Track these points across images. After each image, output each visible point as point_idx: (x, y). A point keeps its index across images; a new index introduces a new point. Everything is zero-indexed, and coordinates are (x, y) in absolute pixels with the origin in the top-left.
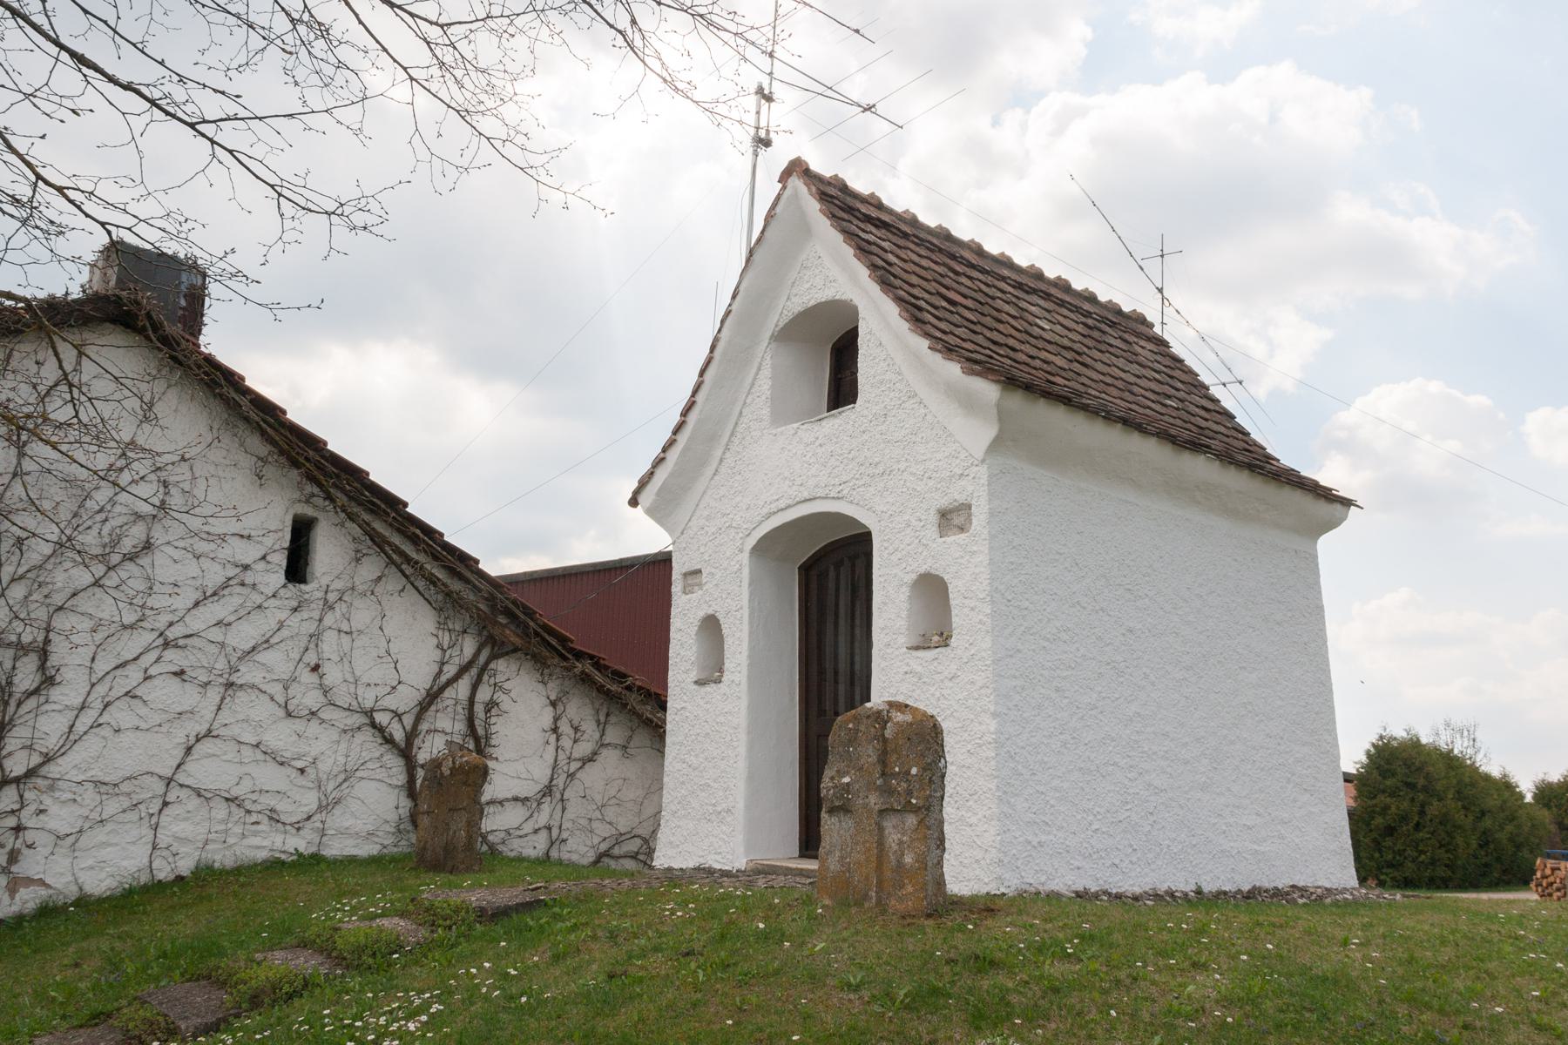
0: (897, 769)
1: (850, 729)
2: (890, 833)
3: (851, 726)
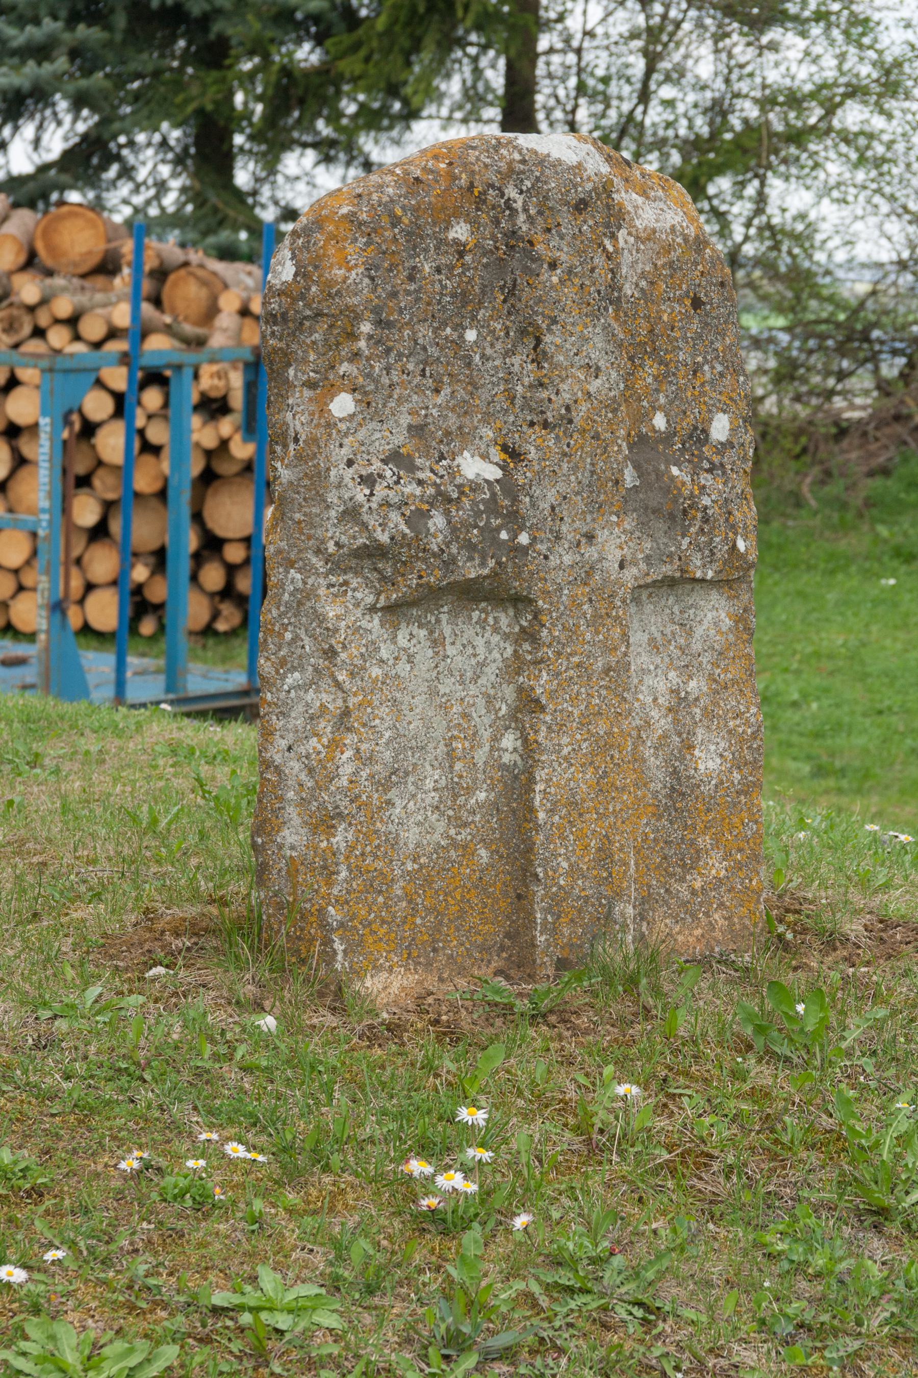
0: (660, 421)
1: (461, 250)
3: (460, 232)
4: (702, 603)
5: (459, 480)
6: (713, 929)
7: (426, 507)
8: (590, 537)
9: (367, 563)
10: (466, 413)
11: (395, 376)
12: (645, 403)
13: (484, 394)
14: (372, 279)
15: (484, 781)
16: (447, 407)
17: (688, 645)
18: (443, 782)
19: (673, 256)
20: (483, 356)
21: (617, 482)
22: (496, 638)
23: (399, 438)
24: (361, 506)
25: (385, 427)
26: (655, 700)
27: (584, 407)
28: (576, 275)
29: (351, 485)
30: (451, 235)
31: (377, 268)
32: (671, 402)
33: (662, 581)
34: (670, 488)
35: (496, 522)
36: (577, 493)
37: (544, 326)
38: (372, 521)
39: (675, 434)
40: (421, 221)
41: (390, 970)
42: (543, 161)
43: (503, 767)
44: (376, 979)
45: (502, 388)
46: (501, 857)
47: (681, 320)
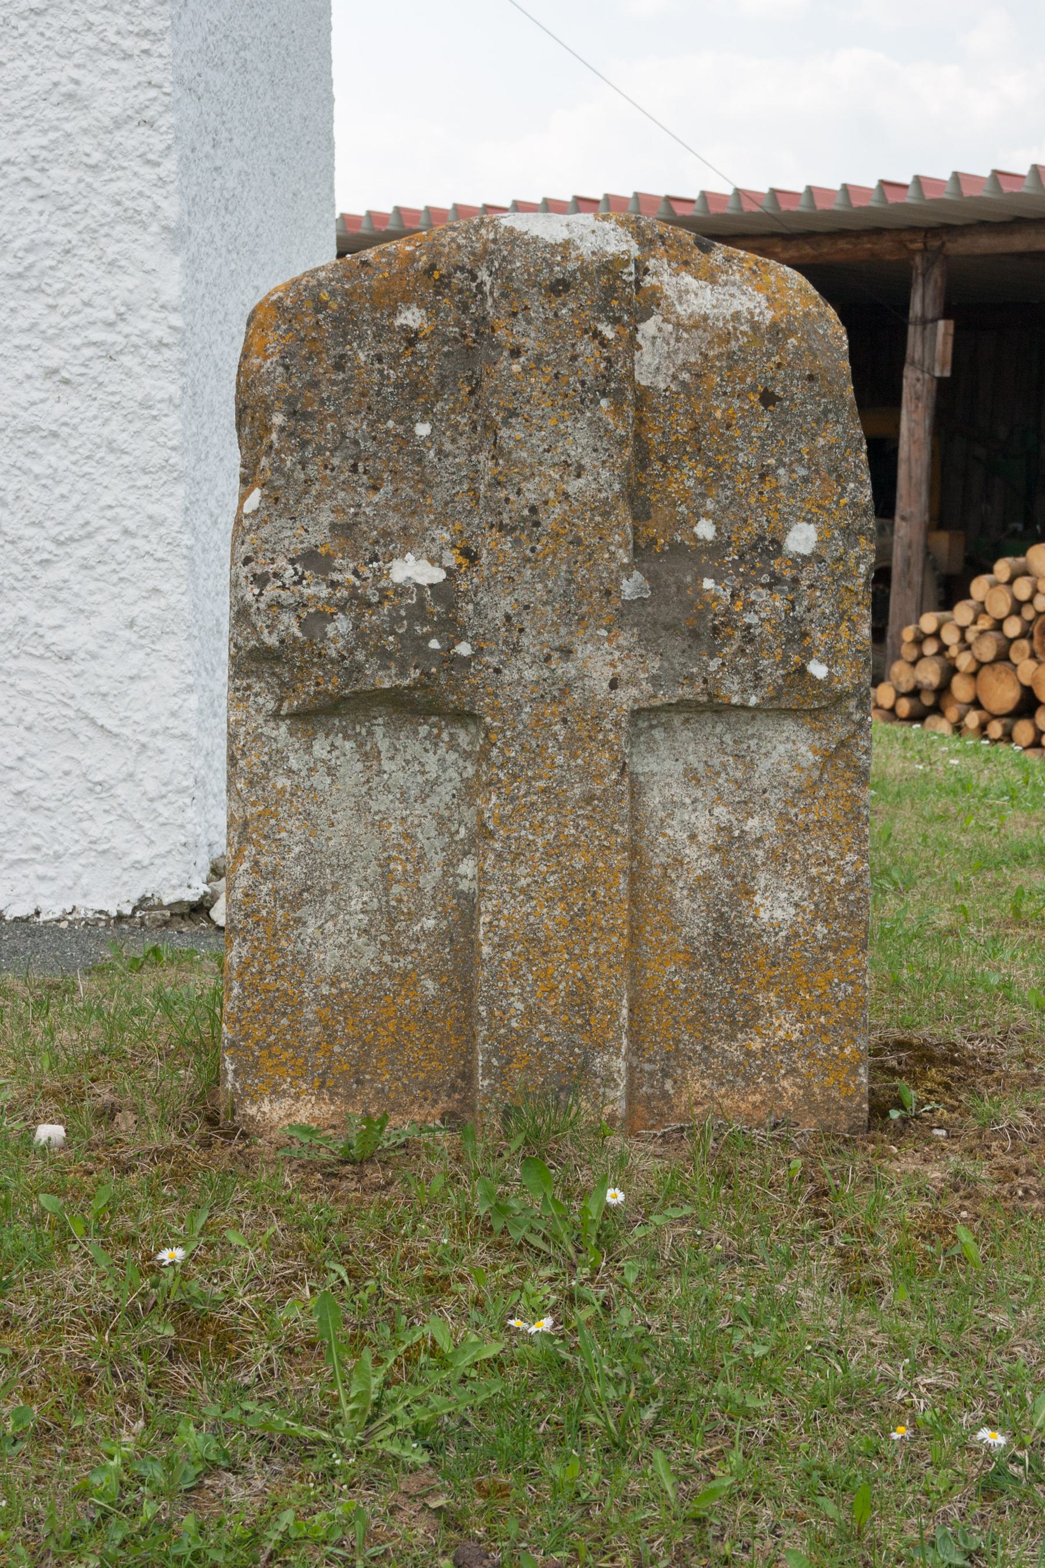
1: (411, 338)
2: (672, 805)
3: (411, 317)
4: (769, 734)
5: (383, 583)
6: (781, 1097)
7: (329, 610)
8: (567, 652)
9: (265, 667)
10: (414, 513)
11: (312, 470)
12: (682, 509)
13: (441, 494)
14: (287, 368)
15: (433, 908)
16: (387, 506)
17: (748, 780)
18: (375, 905)
19: (734, 345)
20: (440, 452)
21: (608, 593)
22: (452, 756)
23: (318, 536)
24: (251, 606)
25: (298, 524)
26: (693, 837)
27: (558, 510)
28: (548, 363)
29: (244, 583)
30: (399, 321)
31: (292, 356)
32: (724, 509)
33: (678, 704)
34: (698, 605)
35: (420, 630)
36: (545, 604)
37: (499, 419)
38: (260, 622)
39: (729, 544)
40: (355, 307)
41: (297, 1098)
42: (516, 239)
43: (460, 895)
44: (276, 1105)
45: (465, 487)
46: (455, 991)
47: (742, 417)
